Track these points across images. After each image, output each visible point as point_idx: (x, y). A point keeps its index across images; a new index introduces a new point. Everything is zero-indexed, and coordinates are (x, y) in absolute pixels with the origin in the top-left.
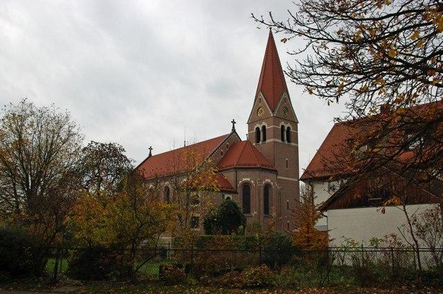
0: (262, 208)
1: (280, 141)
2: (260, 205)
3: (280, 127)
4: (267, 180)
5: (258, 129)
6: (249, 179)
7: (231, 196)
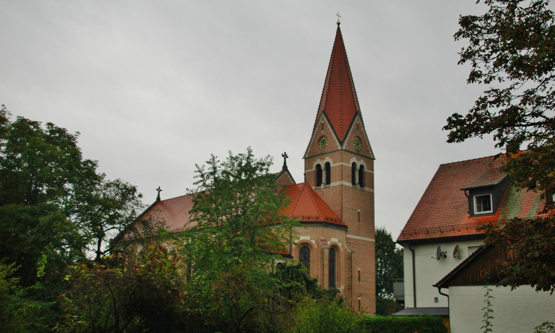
1: (350, 185)
3: (350, 165)
5: (319, 166)
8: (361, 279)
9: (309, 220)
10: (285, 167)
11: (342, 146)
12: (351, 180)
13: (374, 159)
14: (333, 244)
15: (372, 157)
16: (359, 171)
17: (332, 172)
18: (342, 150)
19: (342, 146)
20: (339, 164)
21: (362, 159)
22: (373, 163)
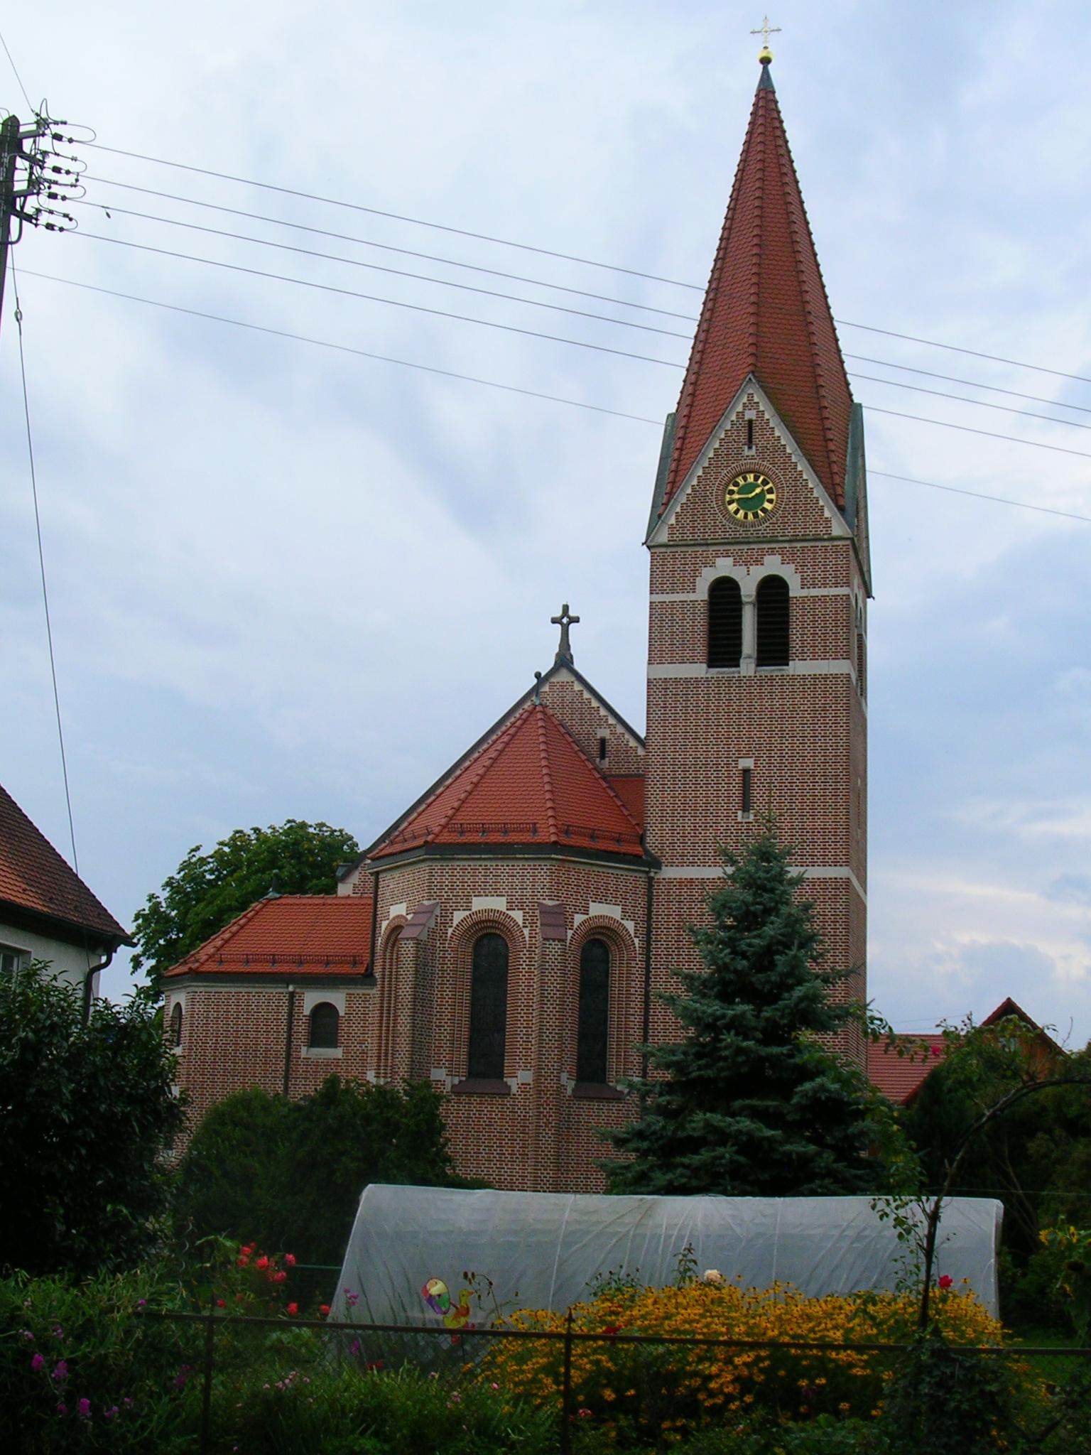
3: (702, 593)
7: (338, 999)
10: (564, 660)
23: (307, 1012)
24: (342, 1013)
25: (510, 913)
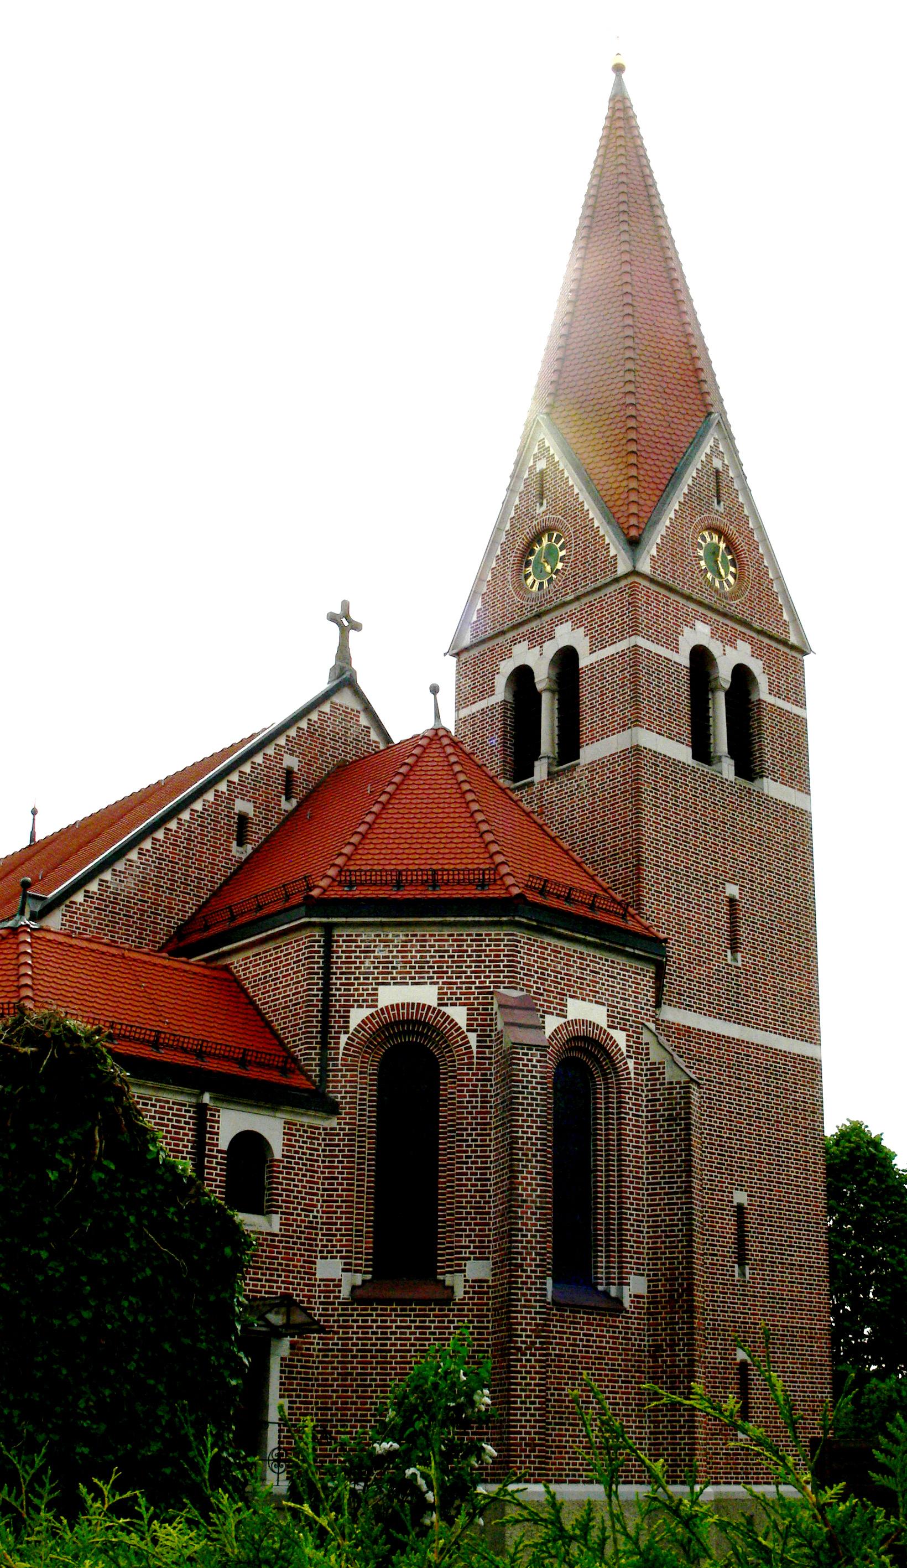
0: (533, 1227)
1: (682, 753)
2: (351, 885)
3: (683, 659)
4: (579, 1010)
5: (523, 676)
6: (427, 995)
7: (271, 1127)
8: (753, 1246)
9: (431, 894)
10: (344, 680)
11: (634, 560)
12: (686, 729)
13: (803, 651)
14: (582, 1031)
15: (793, 640)
16: (730, 695)
17: (587, 694)
18: (634, 573)
19: (634, 560)
20: (623, 645)
21: (744, 638)
22: (799, 669)
23: (224, 1144)
24: (278, 1154)
25: (609, 1030)
